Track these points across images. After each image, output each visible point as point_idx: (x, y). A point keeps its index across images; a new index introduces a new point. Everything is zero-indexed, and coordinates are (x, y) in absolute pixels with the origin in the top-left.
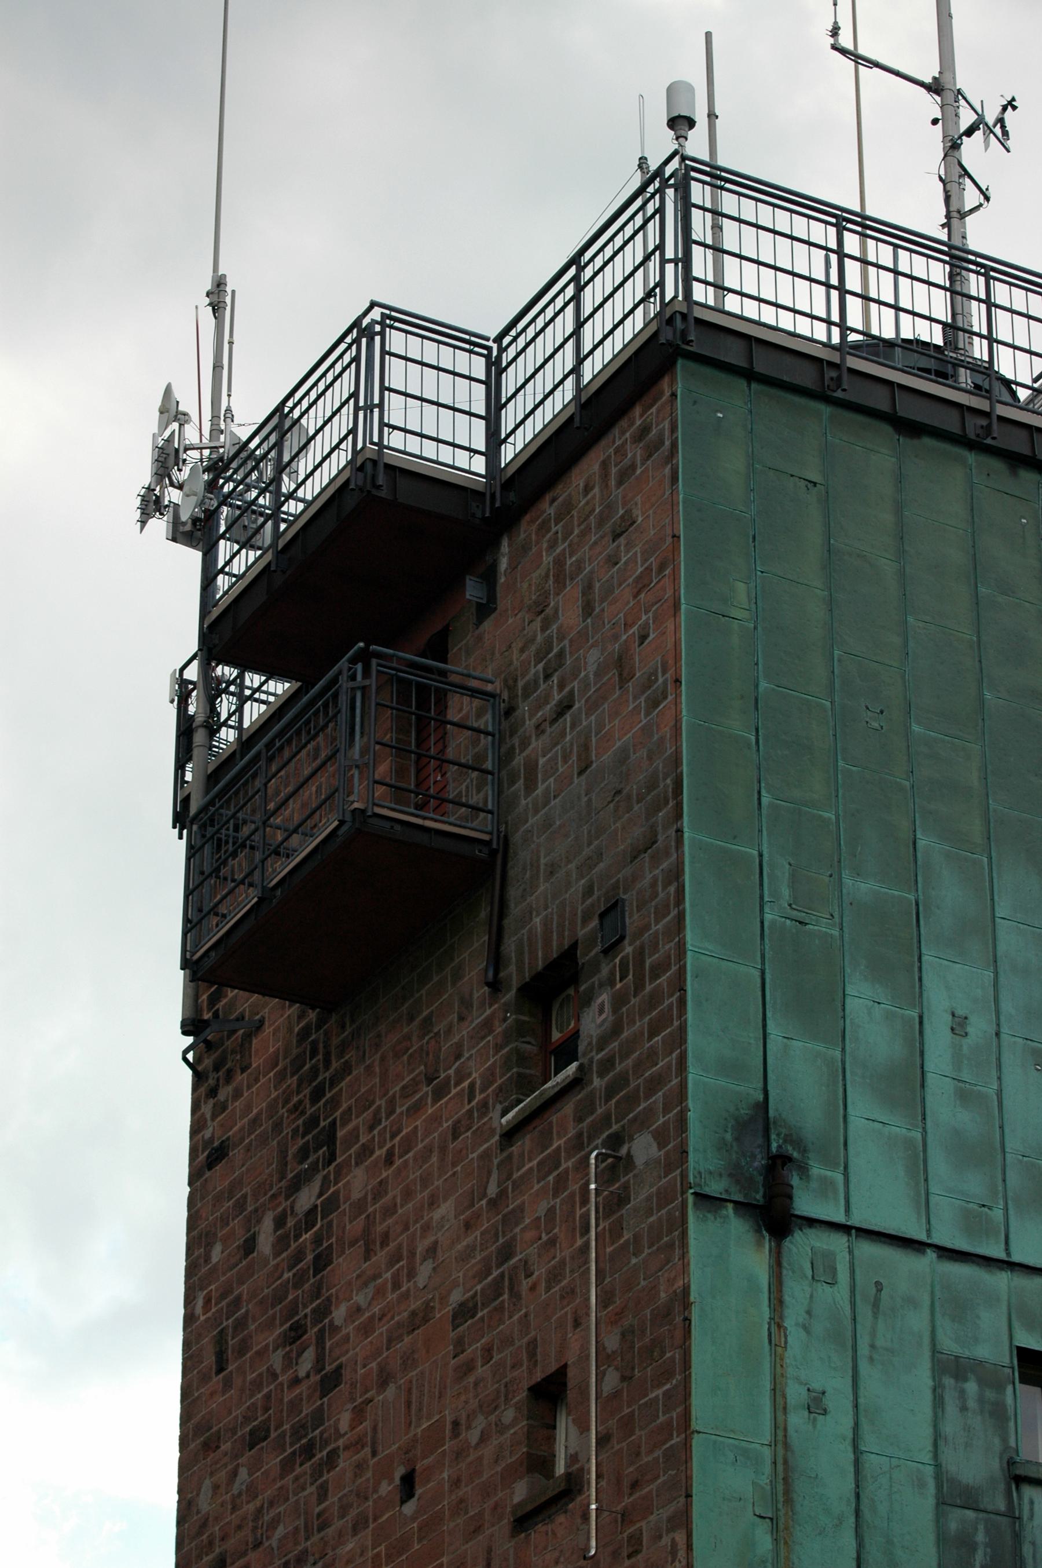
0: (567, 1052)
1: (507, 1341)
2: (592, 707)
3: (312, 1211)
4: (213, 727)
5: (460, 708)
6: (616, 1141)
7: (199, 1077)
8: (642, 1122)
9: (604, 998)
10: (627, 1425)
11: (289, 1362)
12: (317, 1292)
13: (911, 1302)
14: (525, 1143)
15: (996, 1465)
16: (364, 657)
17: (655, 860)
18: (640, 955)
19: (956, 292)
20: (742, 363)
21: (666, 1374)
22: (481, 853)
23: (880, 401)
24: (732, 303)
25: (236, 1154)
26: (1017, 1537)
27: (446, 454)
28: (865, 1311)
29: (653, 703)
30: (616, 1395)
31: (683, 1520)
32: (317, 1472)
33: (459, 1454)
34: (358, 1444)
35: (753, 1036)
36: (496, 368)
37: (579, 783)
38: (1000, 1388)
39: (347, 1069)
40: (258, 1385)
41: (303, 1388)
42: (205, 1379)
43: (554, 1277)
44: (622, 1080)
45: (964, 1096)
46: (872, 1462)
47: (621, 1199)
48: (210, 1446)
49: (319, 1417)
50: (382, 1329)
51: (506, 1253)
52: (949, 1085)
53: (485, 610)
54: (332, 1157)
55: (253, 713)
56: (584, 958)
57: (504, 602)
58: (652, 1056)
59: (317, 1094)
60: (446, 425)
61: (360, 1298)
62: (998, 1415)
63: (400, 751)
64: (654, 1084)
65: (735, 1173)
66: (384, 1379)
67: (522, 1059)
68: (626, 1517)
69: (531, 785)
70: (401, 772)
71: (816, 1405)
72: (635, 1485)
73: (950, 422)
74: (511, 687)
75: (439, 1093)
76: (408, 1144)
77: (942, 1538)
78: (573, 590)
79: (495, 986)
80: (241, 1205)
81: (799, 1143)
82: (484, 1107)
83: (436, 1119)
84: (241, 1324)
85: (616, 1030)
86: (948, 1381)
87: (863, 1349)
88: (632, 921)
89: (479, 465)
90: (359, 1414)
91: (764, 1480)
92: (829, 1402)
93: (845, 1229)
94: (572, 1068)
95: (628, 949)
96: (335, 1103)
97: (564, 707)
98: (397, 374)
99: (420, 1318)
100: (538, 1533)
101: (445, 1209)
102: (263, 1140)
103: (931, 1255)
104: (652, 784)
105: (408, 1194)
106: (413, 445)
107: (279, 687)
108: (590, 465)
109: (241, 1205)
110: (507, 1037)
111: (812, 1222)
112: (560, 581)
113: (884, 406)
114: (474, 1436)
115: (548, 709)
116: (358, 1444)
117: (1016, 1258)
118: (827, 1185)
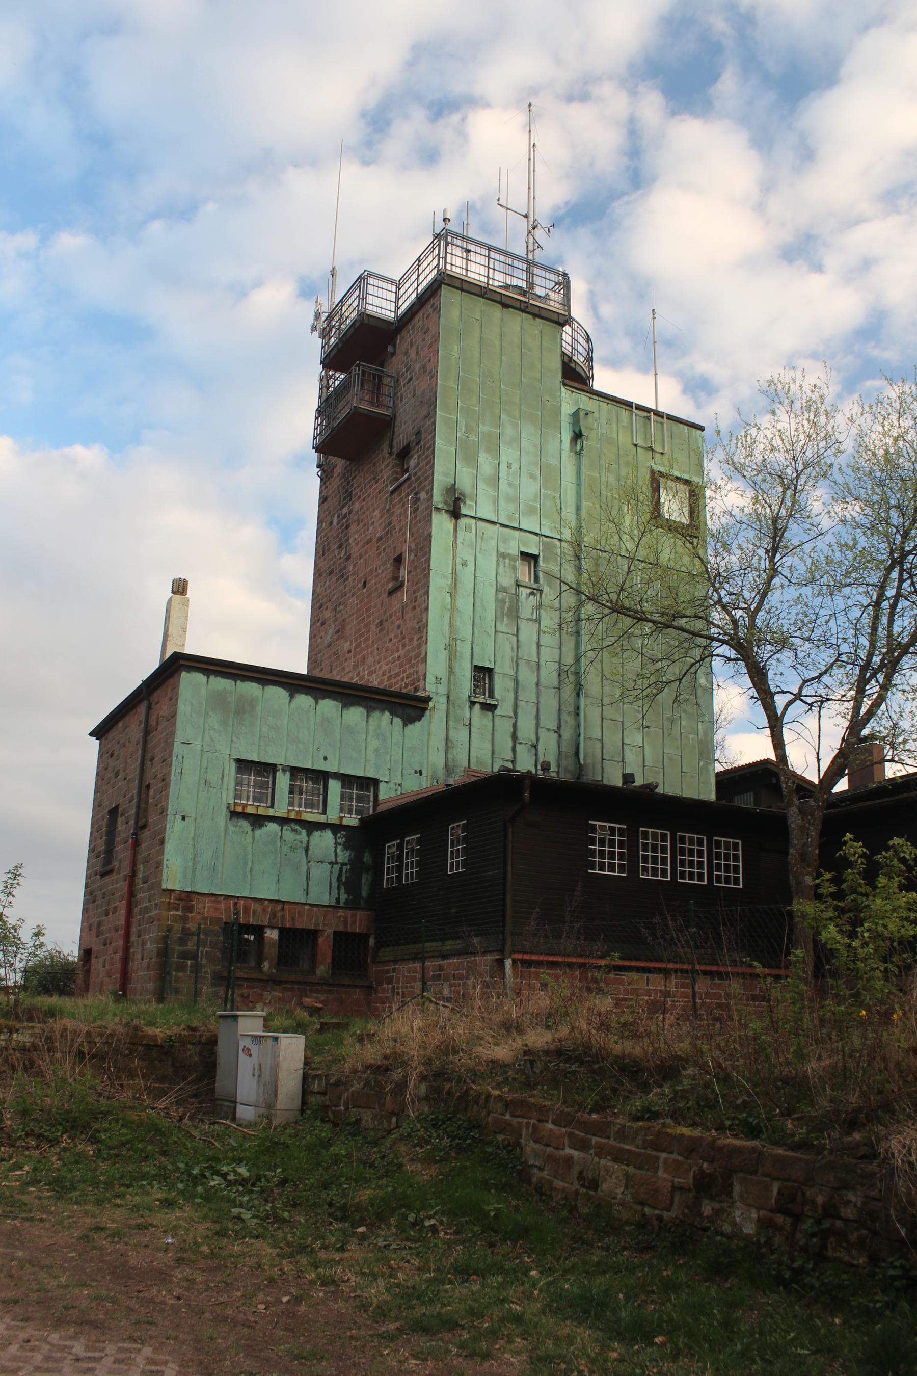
0: (406, 471)
1: (389, 546)
2: (417, 379)
3: (346, 514)
4: (328, 387)
5: (386, 381)
6: (416, 494)
7: (322, 479)
8: (423, 489)
9: (416, 456)
10: (415, 568)
11: (339, 553)
12: (346, 535)
13: (492, 538)
14: (396, 494)
15: (512, 582)
16: (358, 365)
17: (430, 420)
18: (425, 445)
19: (528, 271)
20: (459, 286)
21: (425, 555)
22: (388, 418)
23: (498, 298)
24: (454, 269)
25: (329, 499)
26: (517, 601)
27: (383, 312)
28: (479, 540)
29: (431, 378)
30: (413, 560)
31: (427, 593)
32: (344, 581)
33: (377, 576)
34: (354, 574)
35: (453, 466)
36: (398, 288)
37: (413, 400)
38: (515, 561)
39: (355, 476)
40: (332, 559)
41: (342, 560)
42: (320, 558)
43: (401, 529)
44: (419, 478)
45: (510, 485)
46: (478, 579)
47: (417, 509)
48: (320, 575)
49: (345, 568)
50: (361, 544)
51: (390, 523)
52: (506, 482)
53: (393, 354)
54: (351, 500)
55: (337, 383)
56: (412, 445)
57: (398, 352)
58: (426, 472)
59: (349, 483)
60: (384, 304)
61: (356, 536)
62: (514, 568)
63: (373, 393)
64: (426, 478)
65: (446, 503)
66: (361, 557)
67: (396, 473)
68: (414, 592)
69: (401, 401)
70: (373, 398)
71: (464, 564)
72: (417, 584)
73: (517, 305)
74: (398, 374)
75: (376, 482)
76: (368, 496)
77: (496, 599)
78: (414, 348)
79: (391, 453)
80: (330, 513)
81: (463, 495)
82: (387, 485)
83: (375, 489)
84: (328, 544)
85: (418, 464)
86: (501, 559)
87: (478, 550)
88: (423, 436)
89: (392, 315)
90: (354, 566)
91: (449, 583)
92: (468, 563)
93: (475, 518)
94: (407, 475)
95: (422, 443)
96: (352, 485)
97: (411, 379)
98: (371, 289)
99: (370, 541)
100: (393, 597)
101: (377, 512)
102: (336, 496)
103: (498, 526)
104: (430, 399)
105: (368, 509)
106: (375, 309)
107: (343, 376)
108: (420, 315)
109: (330, 513)
110: (393, 467)
111: (466, 516)
112: (411, 345)
113: (499, 299)
114: (380, 572)
115: (406, 380)
116: (354, 574)
117: (521, 527)
118: (470, 506)
